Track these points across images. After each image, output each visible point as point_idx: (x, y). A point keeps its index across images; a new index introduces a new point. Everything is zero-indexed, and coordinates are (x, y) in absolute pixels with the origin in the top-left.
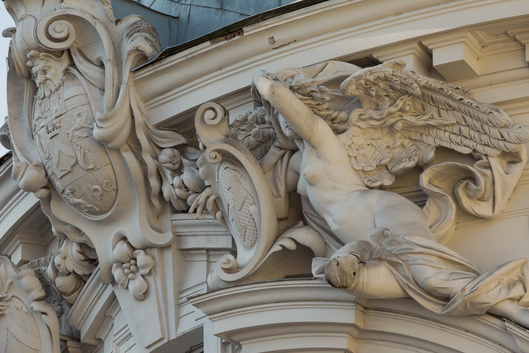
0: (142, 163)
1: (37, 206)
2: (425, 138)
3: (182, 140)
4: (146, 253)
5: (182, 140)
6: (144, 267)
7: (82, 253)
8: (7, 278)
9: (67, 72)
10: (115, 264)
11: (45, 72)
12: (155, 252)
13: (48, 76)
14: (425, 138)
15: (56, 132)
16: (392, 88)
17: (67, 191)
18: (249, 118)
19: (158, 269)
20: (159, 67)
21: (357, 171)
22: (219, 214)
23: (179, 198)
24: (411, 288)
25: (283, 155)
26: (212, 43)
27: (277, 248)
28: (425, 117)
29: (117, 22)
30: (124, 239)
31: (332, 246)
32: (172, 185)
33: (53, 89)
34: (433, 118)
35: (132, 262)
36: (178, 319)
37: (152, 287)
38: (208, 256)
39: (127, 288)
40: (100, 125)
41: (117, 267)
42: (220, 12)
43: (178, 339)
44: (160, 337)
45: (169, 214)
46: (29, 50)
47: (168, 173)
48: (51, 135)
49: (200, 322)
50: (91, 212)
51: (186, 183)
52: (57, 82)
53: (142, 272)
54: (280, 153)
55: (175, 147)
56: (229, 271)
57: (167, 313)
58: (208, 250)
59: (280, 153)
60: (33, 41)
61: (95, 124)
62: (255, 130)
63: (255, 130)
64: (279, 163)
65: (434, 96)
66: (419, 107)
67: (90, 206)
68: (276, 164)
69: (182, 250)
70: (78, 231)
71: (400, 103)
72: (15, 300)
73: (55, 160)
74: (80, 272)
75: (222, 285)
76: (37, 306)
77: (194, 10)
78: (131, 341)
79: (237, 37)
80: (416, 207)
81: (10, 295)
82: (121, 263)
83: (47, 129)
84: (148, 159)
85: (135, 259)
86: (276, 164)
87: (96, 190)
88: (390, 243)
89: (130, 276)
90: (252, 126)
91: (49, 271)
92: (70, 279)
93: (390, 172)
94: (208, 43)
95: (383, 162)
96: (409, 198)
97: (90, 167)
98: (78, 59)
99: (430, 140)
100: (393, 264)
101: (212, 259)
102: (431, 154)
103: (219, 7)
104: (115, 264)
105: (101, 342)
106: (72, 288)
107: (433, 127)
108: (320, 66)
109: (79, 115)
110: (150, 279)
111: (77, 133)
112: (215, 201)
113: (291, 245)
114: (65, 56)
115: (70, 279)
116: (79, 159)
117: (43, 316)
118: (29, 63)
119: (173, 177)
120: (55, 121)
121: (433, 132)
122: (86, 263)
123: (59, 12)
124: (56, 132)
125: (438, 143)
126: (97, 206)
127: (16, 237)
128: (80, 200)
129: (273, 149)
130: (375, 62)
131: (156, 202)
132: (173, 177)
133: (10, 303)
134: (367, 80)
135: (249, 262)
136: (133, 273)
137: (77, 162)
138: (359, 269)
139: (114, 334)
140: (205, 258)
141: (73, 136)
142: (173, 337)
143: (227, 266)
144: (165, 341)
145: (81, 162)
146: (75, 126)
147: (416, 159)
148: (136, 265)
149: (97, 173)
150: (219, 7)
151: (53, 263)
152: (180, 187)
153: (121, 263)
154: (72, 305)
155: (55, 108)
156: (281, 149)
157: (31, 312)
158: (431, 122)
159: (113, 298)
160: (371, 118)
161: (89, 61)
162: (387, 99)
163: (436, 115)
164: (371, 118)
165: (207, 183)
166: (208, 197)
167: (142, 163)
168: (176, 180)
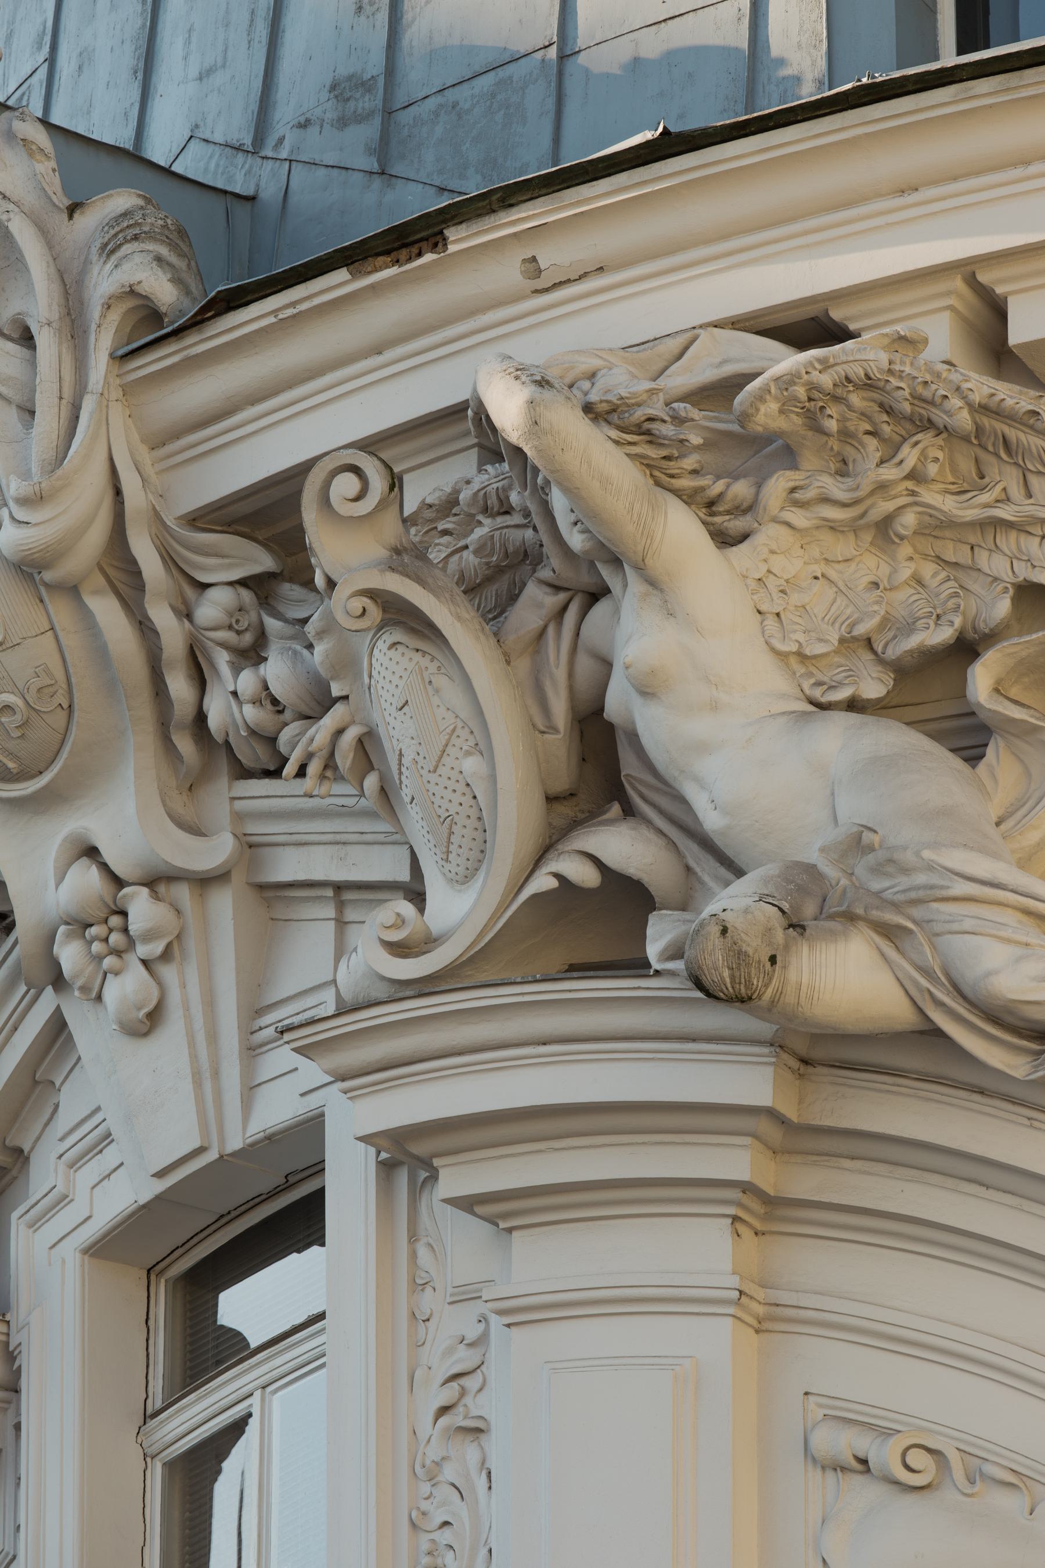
0: (145, 628)
2: (983, 559)
3: (263, 562)
4: (156, 896)
6: (149, 936)
10: (62, 929)
12: (183, 893)
14: (983, 559)
16: (888, 410)
18: (464, 496)
19: (192, 943)
20: (196, 344)
21: (781, 656)
22: (371, 782)
23: (253, 732)
24: (939, 1004)
25: (565, 608)
26: (355, 275)
27: (543, 882)
28: (985, 497)
29: (72, 210)
30: (92, 852)
31: (706, 878)
32: (235, 694)
34: (1006, 499)
35: (115, 921)
36: (250, 1089)
37: (174, 997)
38: (340, 906)
39: (99, 998)
40: (21, 514)
41: (69, 936)
42: (377, 182)
43: (249, 1152)
47: (222, 659)
49: (314, 1101)
51: (276, 690)
53: (143, 950)
54: (552, 601)
56: (400, 949)
57: (216, 1074)
58: (339, 887)
59: (552, 601)
62: (479, 532)
63: (479, 532)
64: (551, 631)
65: (1012, 434)
66: (966, 466)
68: (542, 633)
69: (262, 887)
71: (910, 455)
75: (380, 992)
78: (110, 1156)
79: (429, 257)
80: (956, 762)
82: (81, 925)
85: (124, 914)
86: (542, 633)
88: (877, 870)
90: (471, 522)
93: (880, 661)
94: (341, 275)
95: (860, 630)
96: (936, 736)
99: (998, 565)
100: (888, 932)
101: (350, 915)
102: (1003, 607)
103: (376, 167)
104: (62, 929)
107: (1009, 525)
108: (673, 345)
112: (360, 742)
113: (585, 875)
119: (237, 670)
121: (1008, 541)
125: (1024, 573)
129: (532, 591)
130: (836, 334)
131: (185, 745)
132: (237, 670)
134: (813, 387)
135: (461, 924)
136: (118, 953)
138: (787, 947)
139: (60, 1135)
140: (330, 912)
142: (235, 1143)
143: (395, 936)
144: (212, 1156)
147: (958, 621)
150: (376, 167)
152: (256, 702)
153: (81, 925)
156: (557, 588)
158: (1004, 513)
159: (58, 1027)
160: (826, 500)
162: (872, 443)
163: (1016, 492)
164: (826, 500)
165: (336, 690)
166: (340, 732)
168: (247, 681)
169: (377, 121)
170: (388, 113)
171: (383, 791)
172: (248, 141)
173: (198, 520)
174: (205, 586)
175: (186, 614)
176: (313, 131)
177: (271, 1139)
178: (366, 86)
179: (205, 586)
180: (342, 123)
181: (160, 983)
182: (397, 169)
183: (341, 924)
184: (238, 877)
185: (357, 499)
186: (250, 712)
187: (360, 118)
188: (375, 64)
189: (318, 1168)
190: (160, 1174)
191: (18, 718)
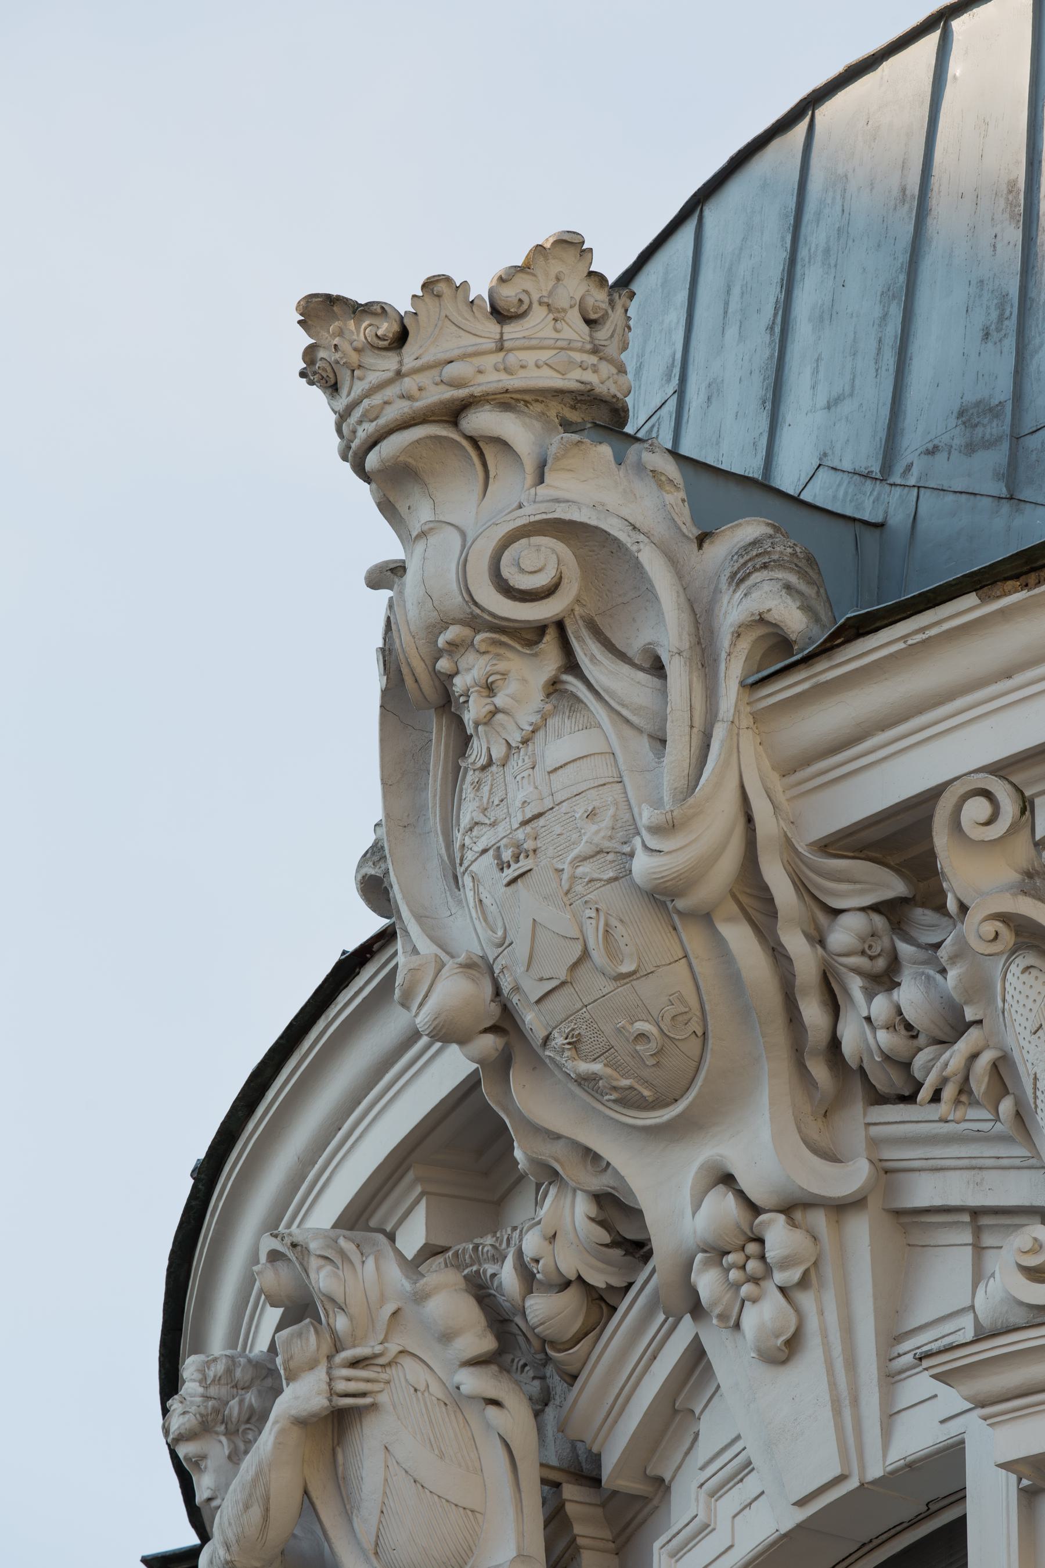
0: (778, 955)
1: (470, 1087)
3: (895, 887)
4: (792, 1223)
5: (895, 887)
6: (786, 1263)
7: (602, 1223)
8: (383, 1300)
9: (554, 688)
10: (700, 1256)
11: (490, 689)
12: (819, 1220)
13: (500, 700)
15: (524, 864)
17: (559, 1040)
19: (829, 1270)
20: (827, 670)
22: (1006, 1106)
26: (984, 600)
29: (701, 540)
30: (728, 1179)
32: (868, 1019)
33: (515, 738)
35: (752, 1248)
36: (889, 1417)
37: (812, 1324)
38: (978, 1231)
39: (737, 1326)
40: (653, 843)
41: (707, 1264)
42: (1006, 507)
44: (837, 1472)
45: (859, 1106)
46: (444, 625)
47: (856, 985)
48: (510, 873)
49: (953, 1428)
50: (629, 1100)
51: (909, 1014)
52: (526, 718)
53: (780, 1277)
55: (875, 908)
57: (855, 1401)
58: (976, 1213)
60: (455, 600)
61: (637, 841)
67: (625, 1082)
70: (591, 1157)
72: (407, 1362)
73: (521, 949)
74: (597, 1280)
75: (1018, 1317)
76: (472, 1381)
77: (927, 500)
78: (751, 1485)
81: (393, 1348)
82: (717, 1253)
83: (498, 856)
84: (795, 943)
85: (761, 1241)
87: (642, 1036)
89: (746, 1289)
91: (508, 1276)
92: (570, 1298)
94: (971, 599)
97: (625, 969)
98: (587, 650)
101: (988, 1240)
103: (1004, 492)
104: (700, 1256)
105: (661, 1486)
106: (576, 1326)
109: (591, 815)
110: (806, 1300)
111: (585, 869)
112: (995, 1066)
114: (549, 643)
115: (570, 1298)
116: (591, 944)
117: (491, 1411)
118: (444, 664)
119: (870, 996)
120: (520, 835)
122: (617, 1253)
123: (531, 513)
124: (524, 864)
126: (646, 1082)
127: (410, 1176)
128: (597, 1067)
131: (820, 1071)
132: (870, 996)
133: (392, 1372)
136: (755, 1280)
137: (585, 954)
139: (701, 1462)
140: (967, 1237)
141: (573, 878)
142: (875, 1471)
144: (853, 1484)
145: (598, 955)
146: (581, 849)
148: (762, 1257)
149: (645, 988)
150: (1004, 492)
151: (520, 1253)
152: (890, 1027)
154: (575, 1377)
155: (521, 796)
157: (456, 1399)
159: (696, 1355)
161: (621, 656)
165: (970, 1014)
166: (974, 1056)
167: (778, 955)
168: (880, 1006)
169: (1005, 446)
170: (1016, 438)
171: (1019, 1116)
172: (876, 469)
173: (830, 846)
174: (837, 912)
175: (819, 940)
176: (941, 457)
177: (911, 1467)
178: (994, 411)
179: (837, 912)
180: (970, 448)
181: (797, 1310)
182: (1026, 494)
183: (979, 1249)
184: (874, 1203)
185: (988, 823)
186: (883, 1037)
187: (988, 444)
188: (1002, 390)
189: (959, 1496)
190: (801, 1503)
191: (653, 1046)
